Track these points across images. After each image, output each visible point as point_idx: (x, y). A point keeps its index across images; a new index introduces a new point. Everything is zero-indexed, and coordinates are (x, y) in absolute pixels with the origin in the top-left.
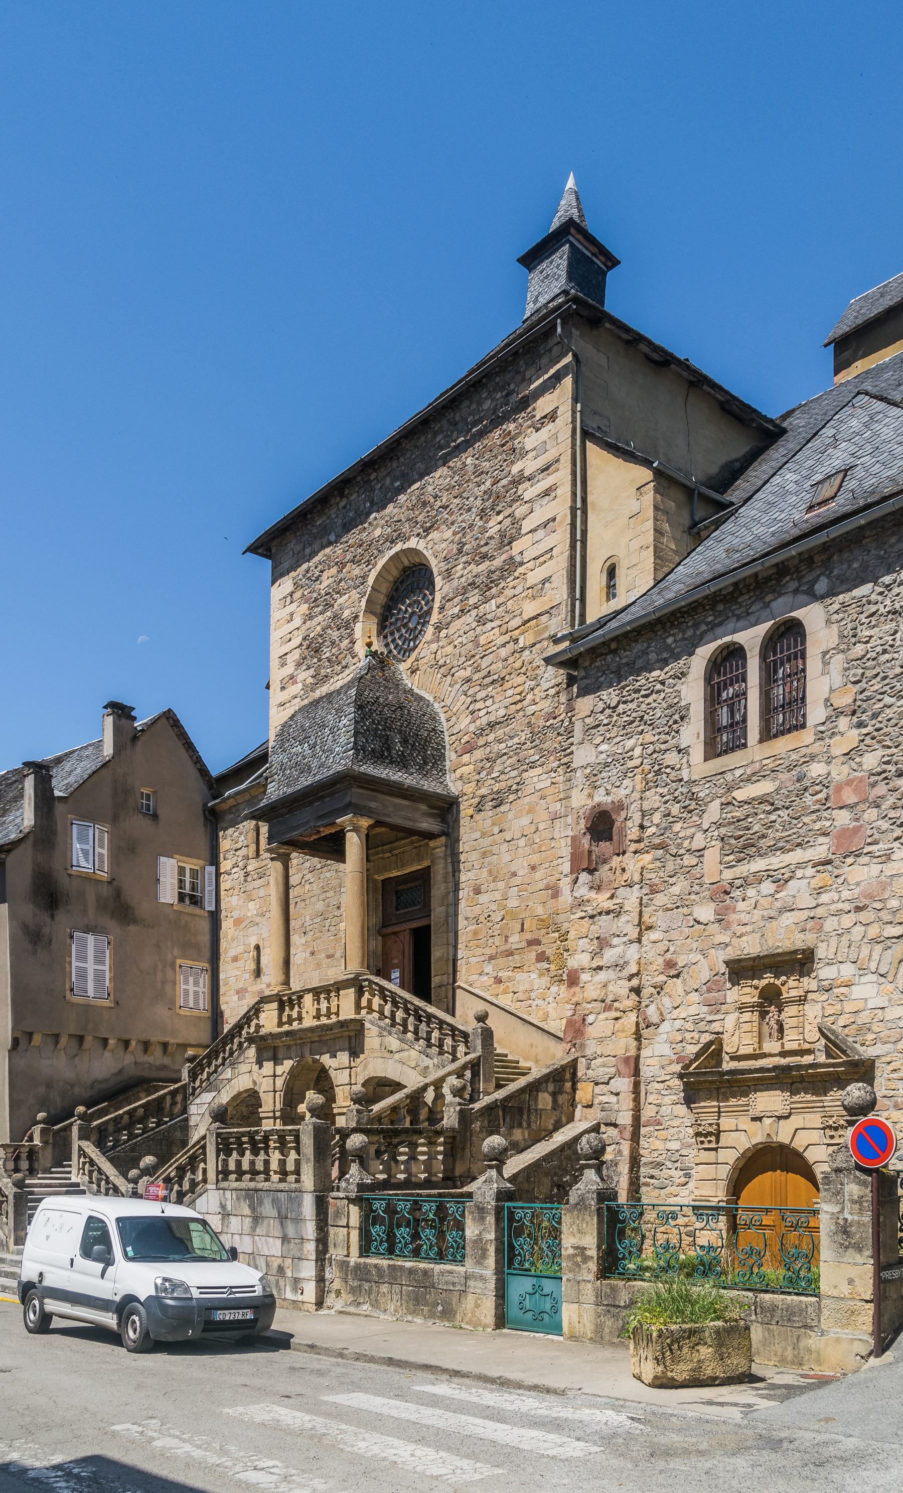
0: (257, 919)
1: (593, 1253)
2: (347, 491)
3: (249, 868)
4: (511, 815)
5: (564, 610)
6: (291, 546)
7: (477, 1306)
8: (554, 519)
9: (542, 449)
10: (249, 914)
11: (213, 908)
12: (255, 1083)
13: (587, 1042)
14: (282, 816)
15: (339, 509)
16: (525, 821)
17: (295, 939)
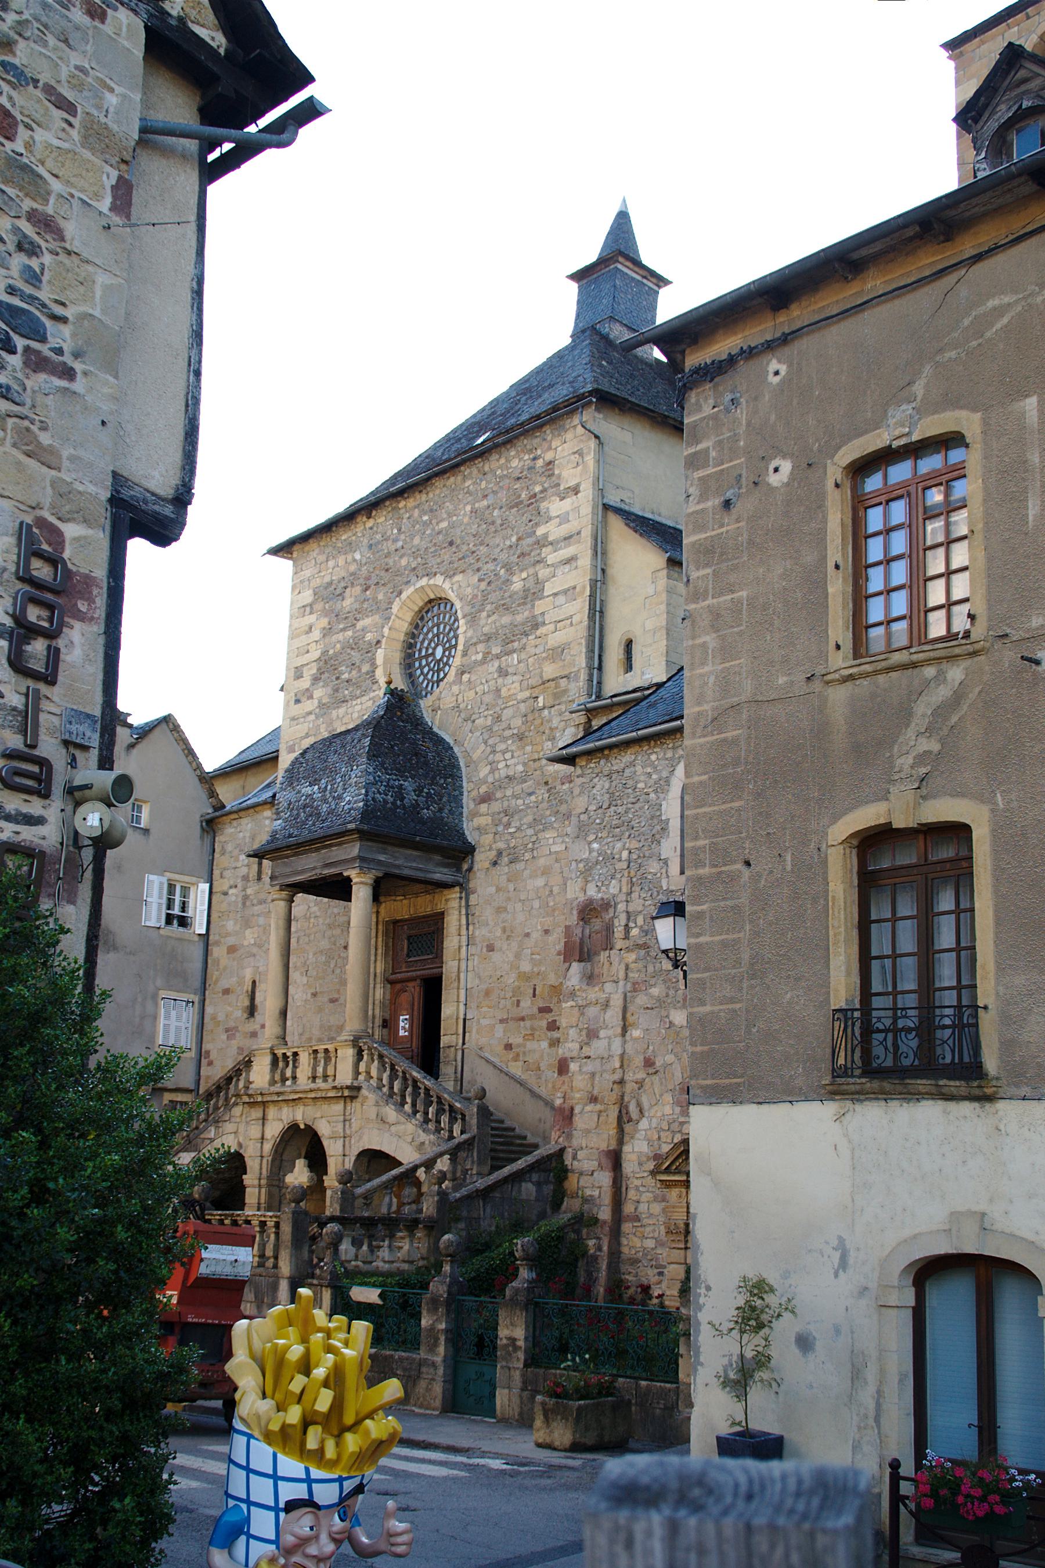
0: (255, 950)
1: (521, 1343)
2: (374, 513)
3: (249, 891)
4: (527, 873)
5: (583, 676)
6: (314, 554)
7: (428, 1390)
8: (574, 588)
9: (564, 519)
10: (246, 943)
11: (204, 932)
12: (240, 1145)
13: (574, 1132)
14: (287, 857)
15: (365, 528)
16: (540, 882)
17: (294, 975)
